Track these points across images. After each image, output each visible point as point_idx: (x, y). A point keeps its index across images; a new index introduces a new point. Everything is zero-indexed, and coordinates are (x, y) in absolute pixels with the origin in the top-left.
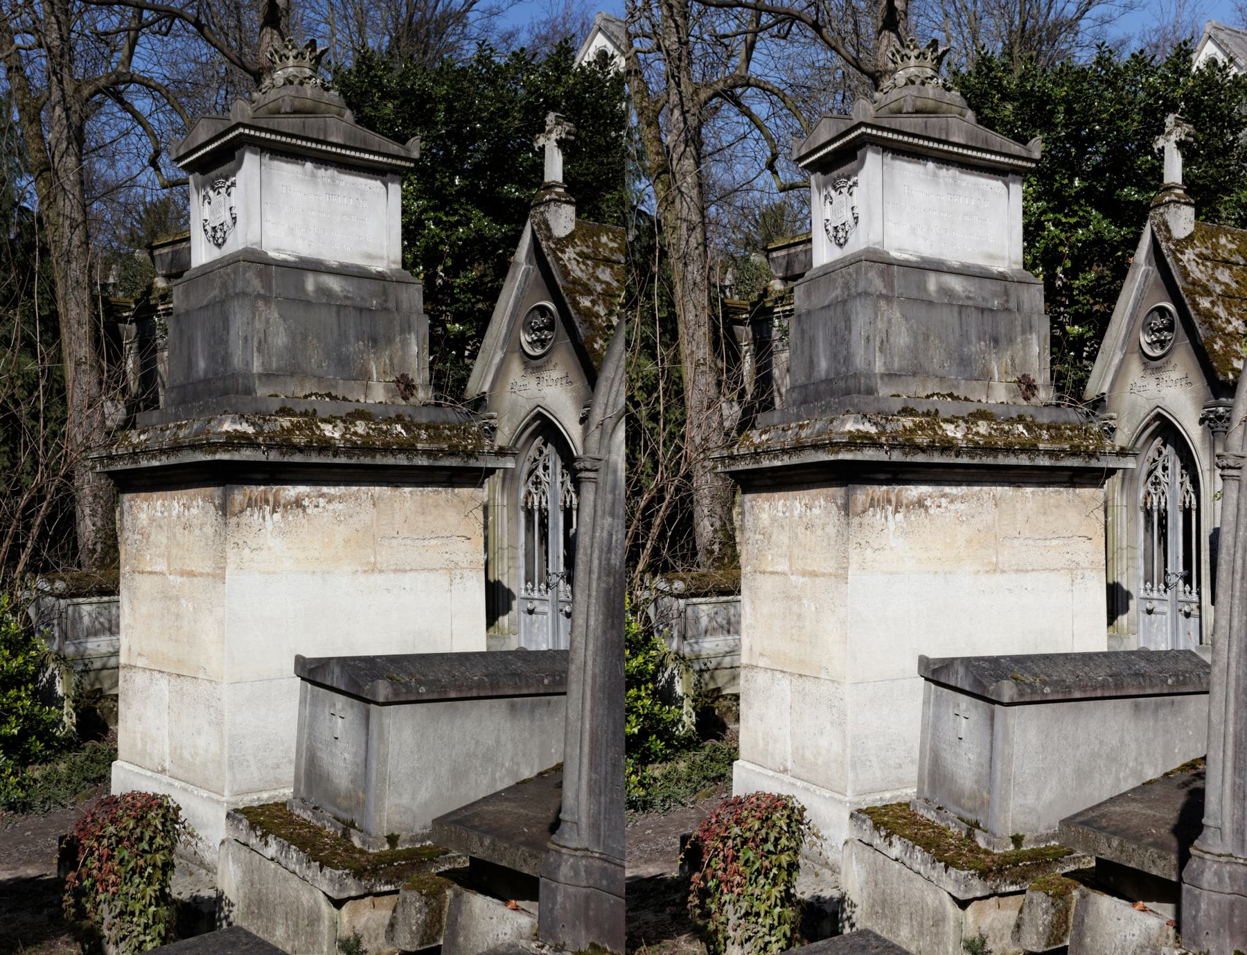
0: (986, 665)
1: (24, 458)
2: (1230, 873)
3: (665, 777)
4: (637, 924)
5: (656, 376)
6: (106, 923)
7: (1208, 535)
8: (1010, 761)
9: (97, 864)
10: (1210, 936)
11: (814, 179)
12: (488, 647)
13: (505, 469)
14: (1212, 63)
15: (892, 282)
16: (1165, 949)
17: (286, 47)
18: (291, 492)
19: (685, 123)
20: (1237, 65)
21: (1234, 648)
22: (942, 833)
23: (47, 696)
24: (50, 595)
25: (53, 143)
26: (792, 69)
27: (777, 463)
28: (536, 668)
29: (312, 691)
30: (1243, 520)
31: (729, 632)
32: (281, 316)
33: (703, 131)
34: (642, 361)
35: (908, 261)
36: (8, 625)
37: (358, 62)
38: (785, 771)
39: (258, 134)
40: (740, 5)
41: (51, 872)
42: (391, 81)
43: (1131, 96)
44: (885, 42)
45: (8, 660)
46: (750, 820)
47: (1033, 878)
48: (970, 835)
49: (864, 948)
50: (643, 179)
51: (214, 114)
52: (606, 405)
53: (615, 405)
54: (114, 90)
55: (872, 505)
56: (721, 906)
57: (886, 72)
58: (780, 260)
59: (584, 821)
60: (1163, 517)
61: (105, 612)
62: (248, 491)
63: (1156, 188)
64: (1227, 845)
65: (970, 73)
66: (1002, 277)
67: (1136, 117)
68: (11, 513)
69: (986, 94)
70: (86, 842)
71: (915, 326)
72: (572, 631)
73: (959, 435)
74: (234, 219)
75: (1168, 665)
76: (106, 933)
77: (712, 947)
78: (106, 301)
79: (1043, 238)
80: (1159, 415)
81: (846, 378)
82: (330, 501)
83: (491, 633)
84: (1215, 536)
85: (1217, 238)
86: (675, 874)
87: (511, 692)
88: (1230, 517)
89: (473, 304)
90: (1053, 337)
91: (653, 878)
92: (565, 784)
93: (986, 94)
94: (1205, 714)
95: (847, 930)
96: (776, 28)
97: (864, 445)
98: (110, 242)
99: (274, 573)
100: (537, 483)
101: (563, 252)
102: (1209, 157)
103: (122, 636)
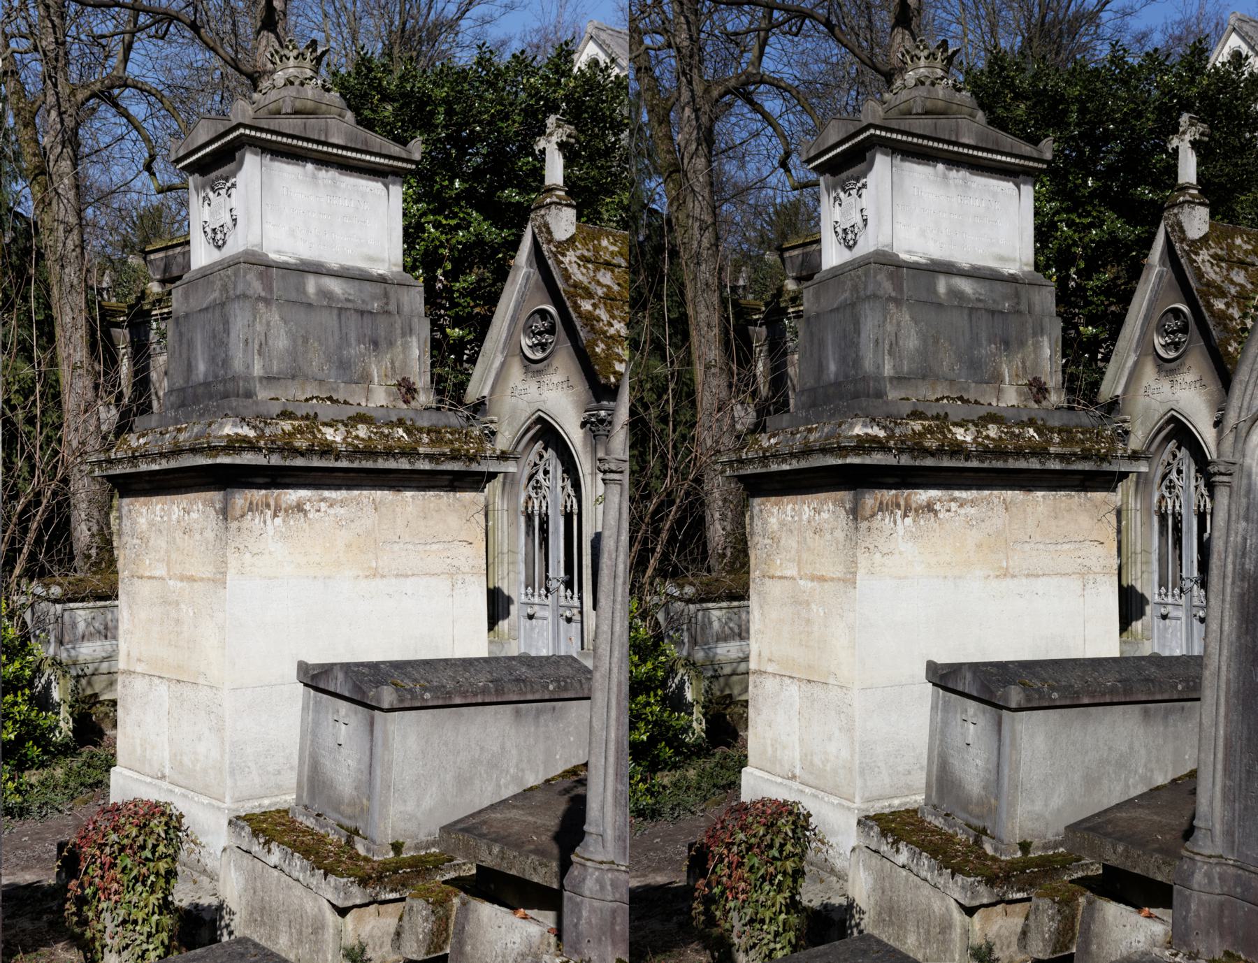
0: (366, 671)
1: (653, 462)
2: (612, 880)
3: (42, 784)
4: (13, 931)
5: (33, 379)
6: (735, 931)
7: (589, 539)
9: (727, 871)
10: (591, 944)
11: (192, 180)
12: (1121, 652)
13: (1139, 473)
14: (594, 63)
15: (902, 284)
16: (546, 957)
17: (918, 47)
19: (62, 124)
20: (619, 65)
22: (321, 840)
23: (43, 702)
24: (680, 599)
25: (683, 144)
26: (170, 70)
27: (155, 467)
28: (540, 673)
29: (944, 696)
31: (106, 637)
32: (912, 318)
33: (80, 132)
34: (19, 364)
35: (287, 263)
37: (990, 62)
38: (163, 777)
39: (889, 135)
40: (118, 5)
41: (681, 879)
42: (1023, 81)
44: (264, 42)
45: (637, 666)
46: (128, 826)
48: (349, 842)
49: (242, 955)
50: (20, 181)
51: (845, 115)
52: (1241, 408)
53: (1249, 409)
54: (744, 91)
55: (250, 510)
56: (726, 913)
57: (265, 72)
58: (158, 263)
59: (1218, 828)
60: (544, 522)
61: (735, 618)
62: (249, 495)
63: (537, 190)
65: (349, 74)
66: (382, 280)
67: (517, 118)
68: (641, 517)
69: (366, 94)
70: (716, 849)
72: (1206, 636)
73: (338, 439)
74: (865, 220)
75: (549, 670)
76: (736, 940)
77: (89, 955)
78: (736, 304)
79: (423, 240)
80: (540, 418)
81: (224, 381)
82: (961, 506)
83: (1124, 638)
84: (597, 540)
85: (599, 241)
86: (52, 882)
89: (1107, 307)
90: (433, 340)
91: (30, 885)
92: (1199, 790)
93: (366, 94)
94: (587, 720)
95: (225, 938)
96: (153, 29)
97: (243, 449)
98: (740, 244)
99: (275, 578)
100: (1171, 487)
101: (1197, 254)
102: (591, 158)
103: (752, 641)
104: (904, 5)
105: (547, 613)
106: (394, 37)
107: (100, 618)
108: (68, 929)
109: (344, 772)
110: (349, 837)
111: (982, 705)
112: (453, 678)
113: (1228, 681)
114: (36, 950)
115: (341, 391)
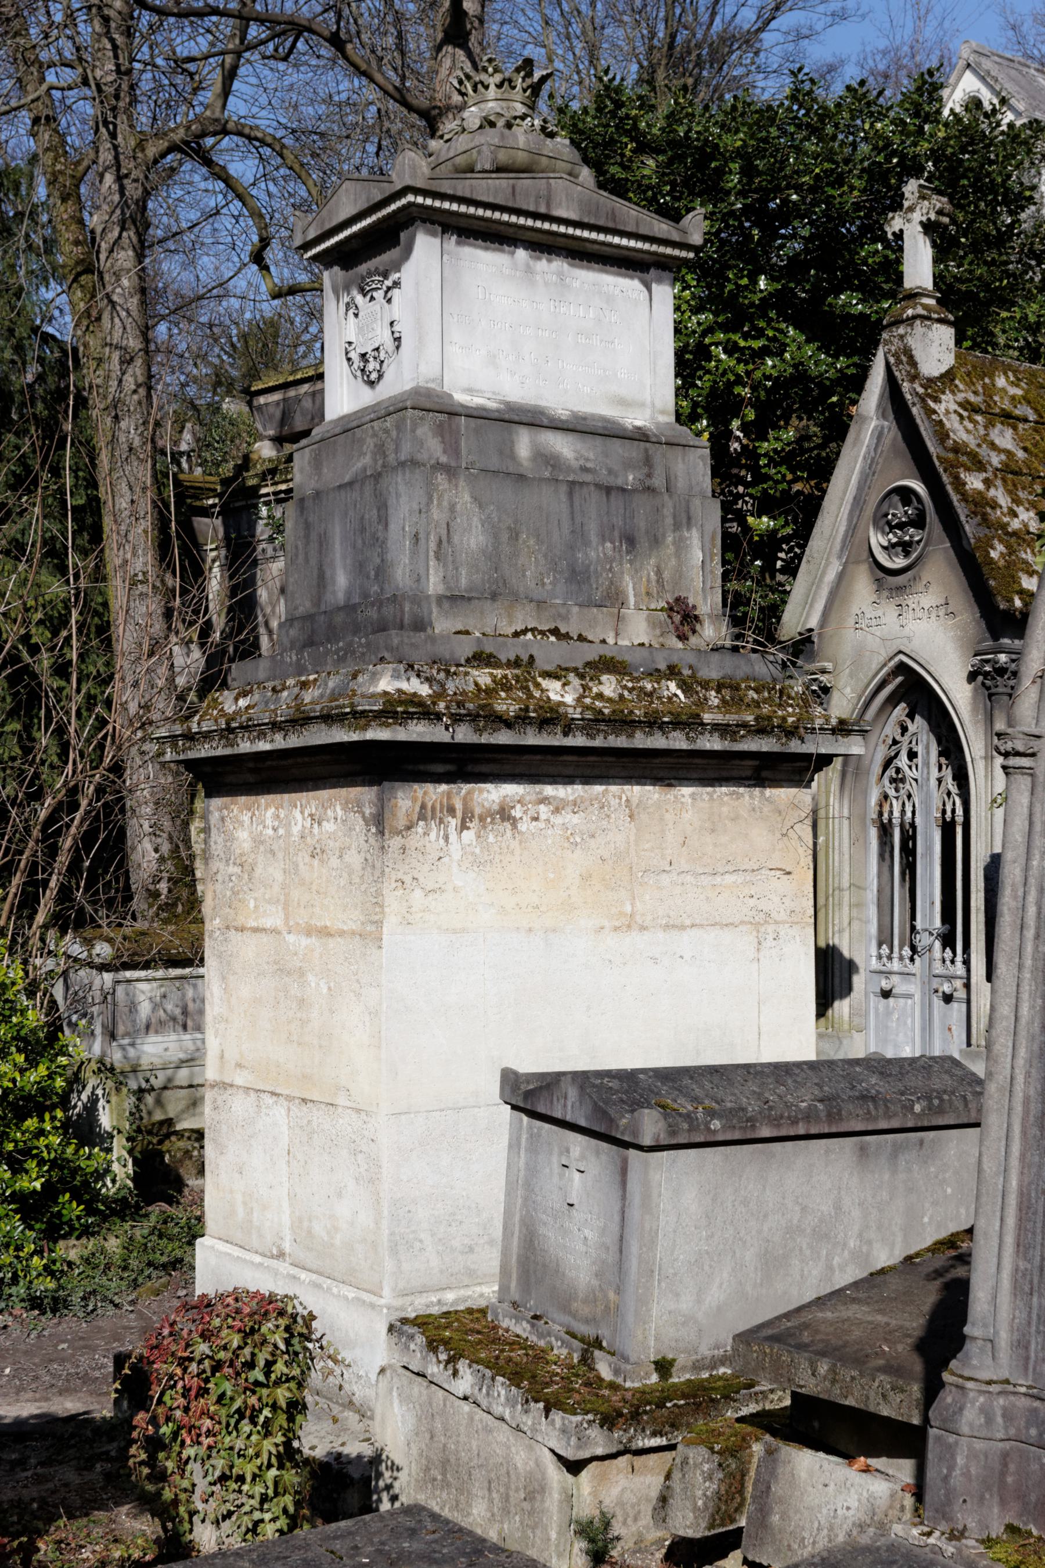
0: (614, 1084)
1: (44, 739)
2: (1005, 1409)
3: (87, 1261)
4: (50, 1485)
5: (66, 602)
7: (981, 866)
8: (653, 1242)
10: (969, 1505)
11: (328, 277)
14: (974, 104)
15: (457, 443)
18: (492, 794)
20: (1012, 108)
21: (1022, 1052)
22: (540, 1356)
23: (84, 1130)
26: (296, 107)
27: (264, 746)
30: (1038, 841)
31: (185, 1027)
33: (150, 205)
34: (45, 577)
35: (485, 409)
36: (23, 1012)
37: (599, 96)
40: (215, 11)
43: (847, 150)
44: (447, 63)
45: (22, 1071)
46: (225, 1332)
47: (688, 1425)
48: (586, 1360)
50: (53, 284)
55: (422, 817)
57: (448, 108)
58: (271, 409)
59: (1004, 1338)
62: (420, 793)
63: (892, 295)
64: (1003, 1366)
65: (585, 110)
66: (640, 436)
67: (856, 182)
71: (495, 516)
74: (398, 340)
75: (914, 1081)
79: (708, 372)
81: (379, 603)
82: (557, 811)
84: (994, 867)
86: (108, 1413)
87: (860, 1127)
88: (1018, 836)
90: (726, 535)
91: (73, 1418)
94: (973, 1160)
95: (385, 1506)
96: (271, 46)
97: (409, 716)
99: (464, 930)
100: (898, 781)
102: (975, 248)
104: (457, 10)
105: (913, 987)
106: (657, 55)
107: (174, 996)
108: (135, 1486)
109: (578, 1247)
110: (585, 1352)
111: (594, 1142)
112: (759, 1096)
113: (1027, 1100)
114: (87, 1515)
115: (574, 619)
